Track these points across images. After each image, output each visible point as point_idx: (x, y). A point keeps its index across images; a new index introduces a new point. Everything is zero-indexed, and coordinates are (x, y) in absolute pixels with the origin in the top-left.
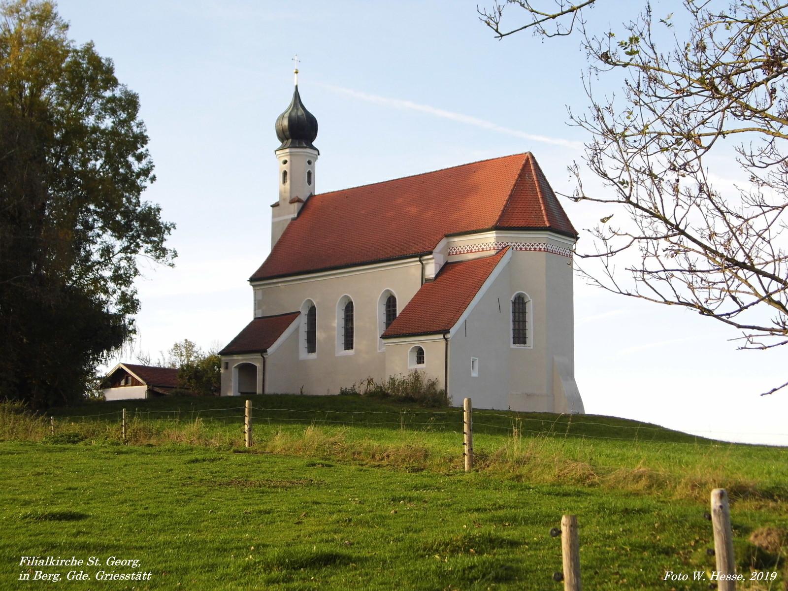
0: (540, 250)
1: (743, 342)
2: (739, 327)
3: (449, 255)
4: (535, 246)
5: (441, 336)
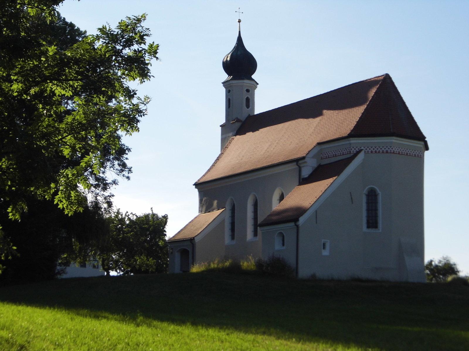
0: (387, 152)
3: (322, 159)
4: (372, 149)
5: (292, 224)
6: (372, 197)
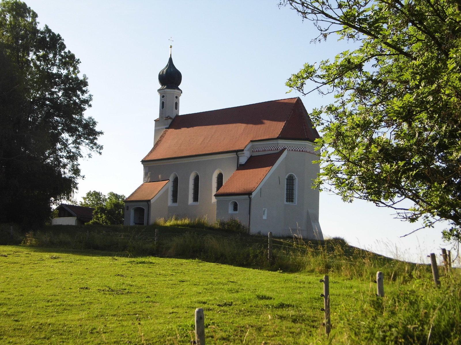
1: (396, 216)
2: (395, 209)
5: (247, 196)
6: (290, 180)
